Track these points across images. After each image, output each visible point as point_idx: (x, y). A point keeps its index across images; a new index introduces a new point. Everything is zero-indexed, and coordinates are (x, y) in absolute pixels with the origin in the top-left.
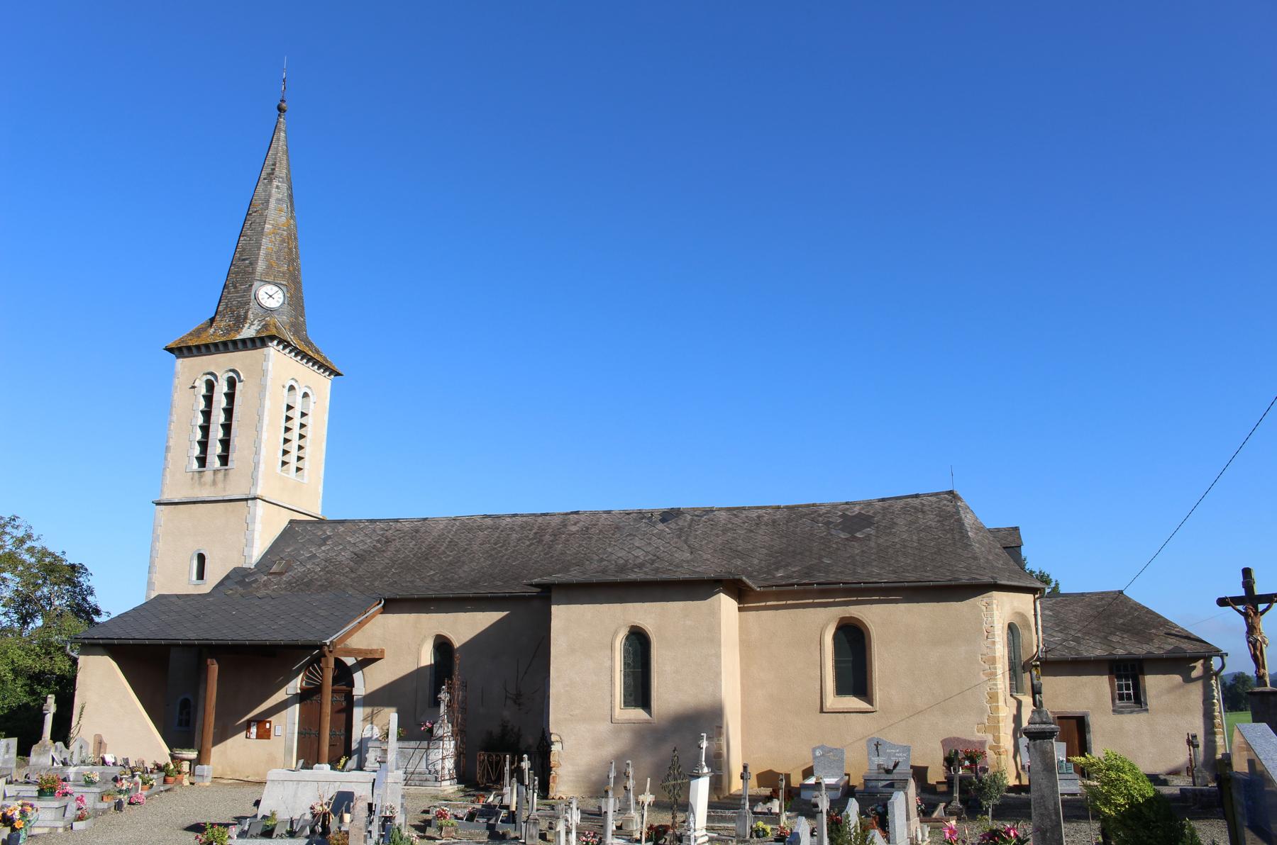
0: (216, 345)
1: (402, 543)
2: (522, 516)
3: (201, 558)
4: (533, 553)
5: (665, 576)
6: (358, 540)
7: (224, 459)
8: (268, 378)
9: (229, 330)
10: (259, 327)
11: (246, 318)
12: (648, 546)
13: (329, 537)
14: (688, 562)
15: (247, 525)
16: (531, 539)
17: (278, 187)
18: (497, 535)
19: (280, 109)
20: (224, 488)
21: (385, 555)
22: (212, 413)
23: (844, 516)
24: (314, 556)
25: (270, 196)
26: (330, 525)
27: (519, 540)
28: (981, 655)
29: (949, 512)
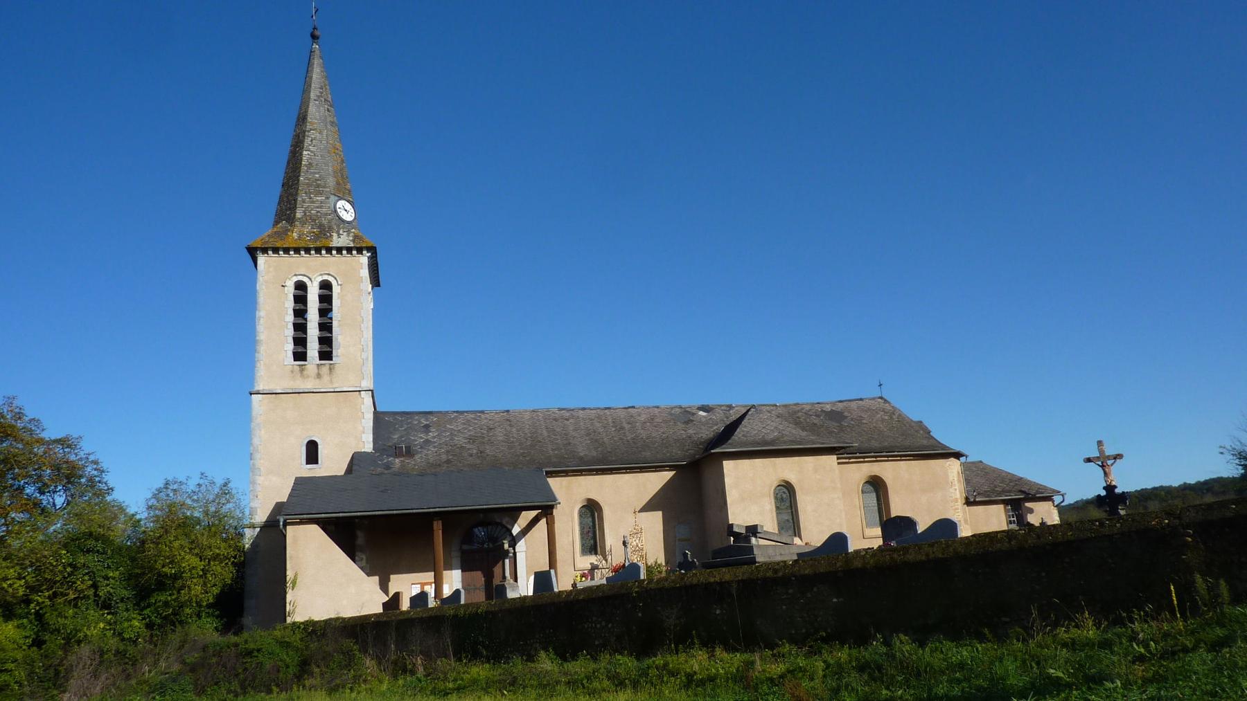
7: (326, 355)
19: (314, 37)
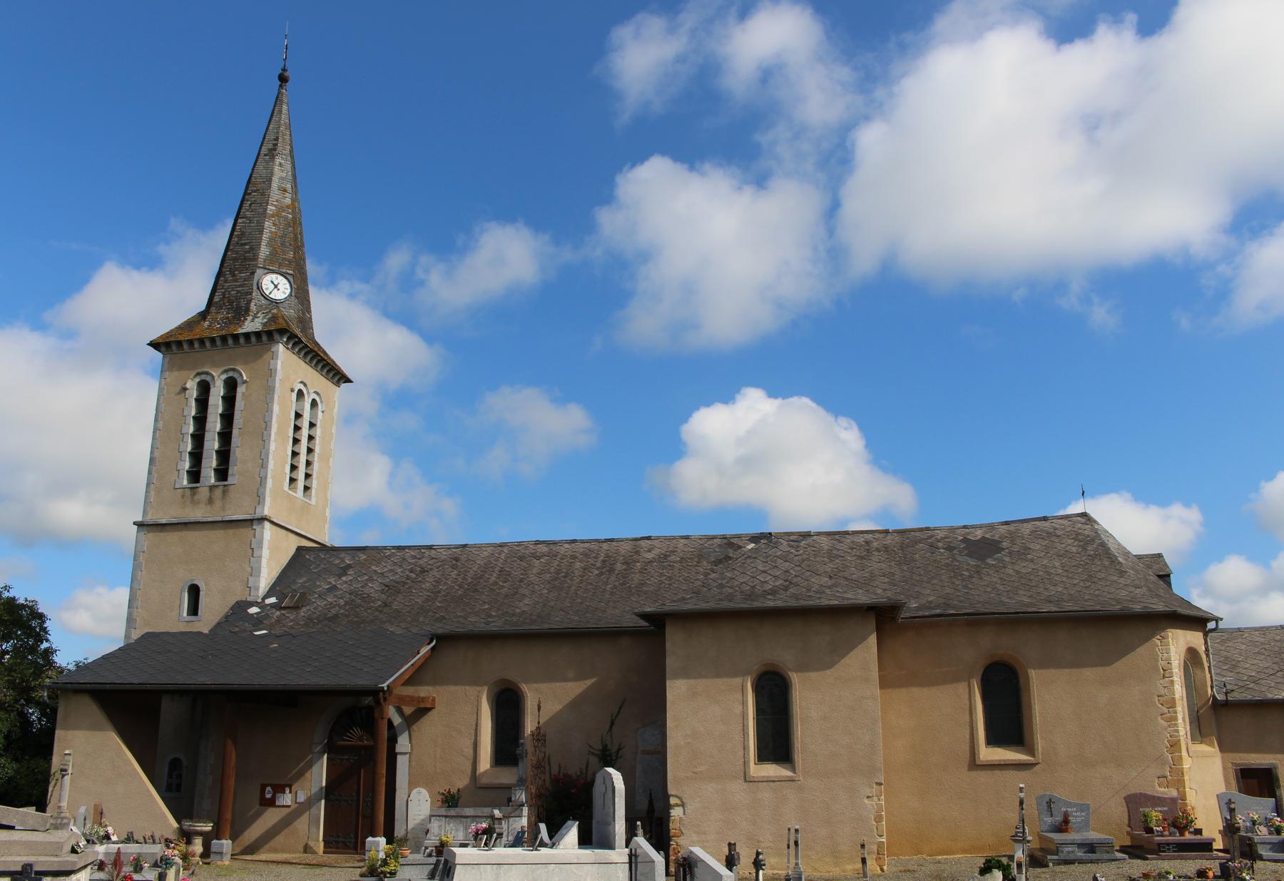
0: (213, 340)
1: (441, 573)
2: (583, 542)
3: (194, 591)
4: (606, 583)
5: (803, 603)
6: (386, 569)
7: (222, 473)
8: (277, 378)
9: (229, 322)
10: (265, 320)
11: (247, 310)
12: (775, 570)
13: (349, 566)
14: (829, 587)
15: (252, 552)
16: (599, 568)
17: (281, 165)
18: (557, 563)
20: (224, 506)
21: (424, 586)
22: (208, 420)
23: (965, 540)
24: (334, 588)
25: (272, 174)
26: (348, 552)
27: (585, 569)
28: (1158, 696)
29: (1088, 536)
